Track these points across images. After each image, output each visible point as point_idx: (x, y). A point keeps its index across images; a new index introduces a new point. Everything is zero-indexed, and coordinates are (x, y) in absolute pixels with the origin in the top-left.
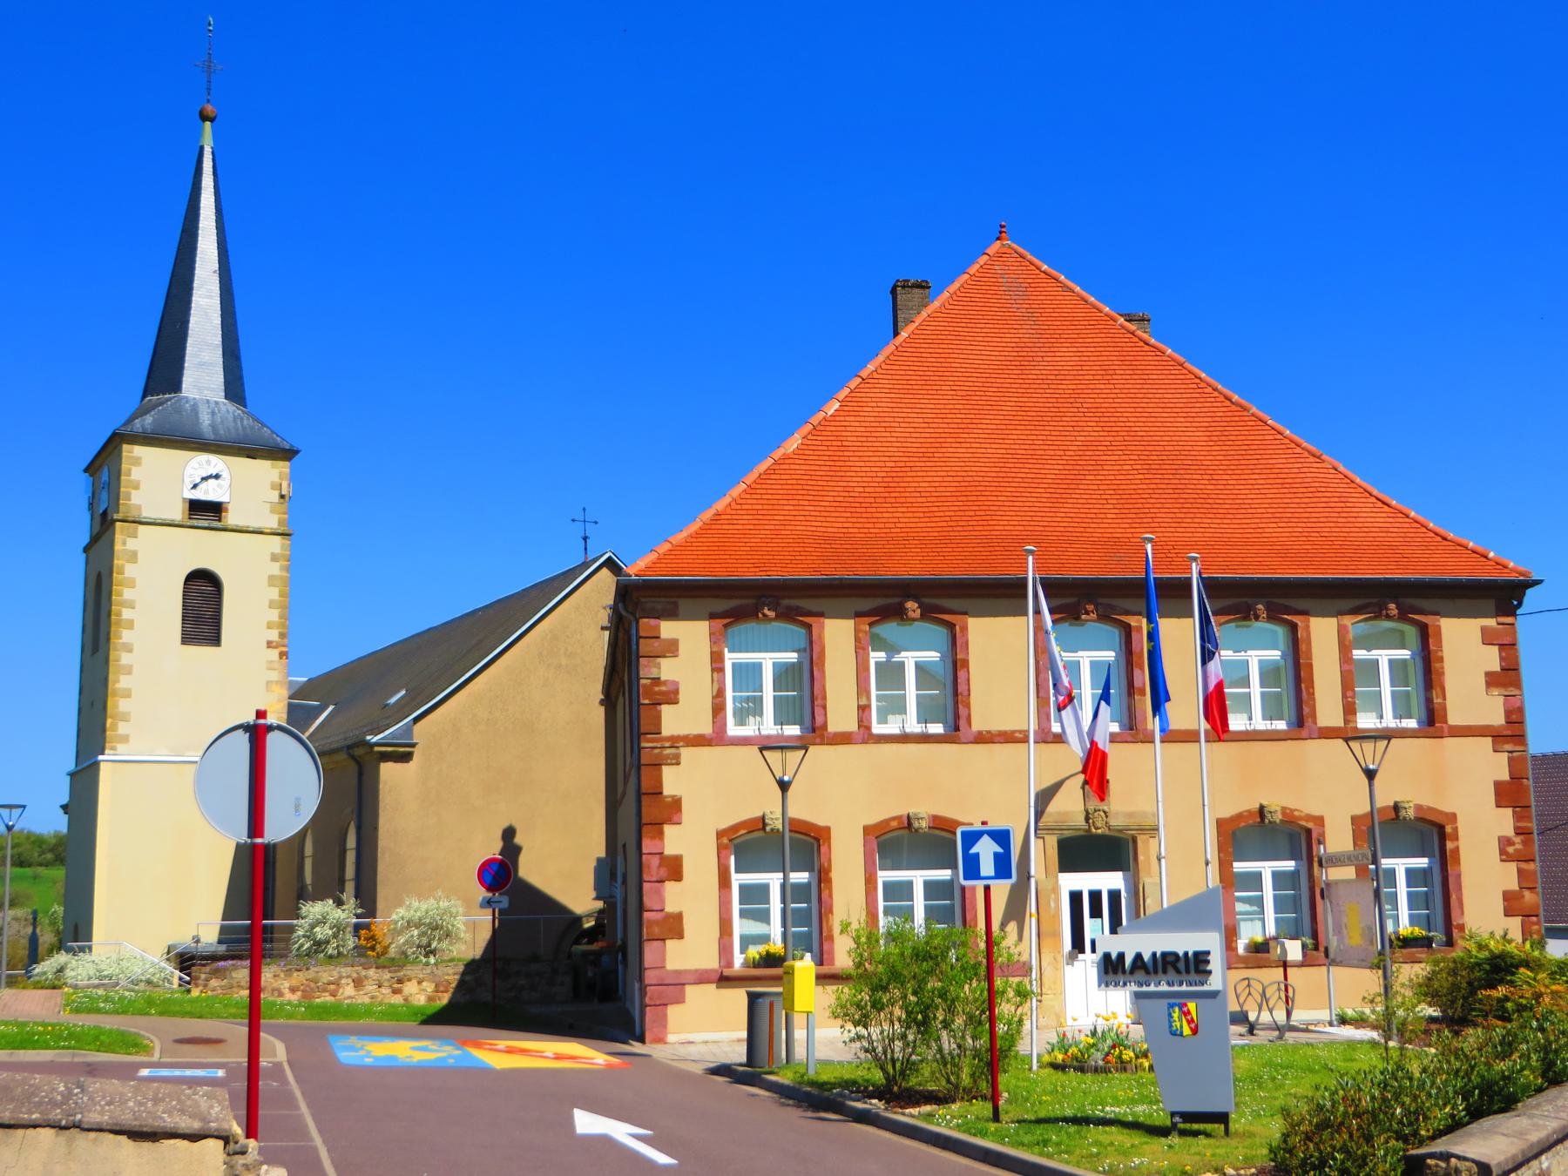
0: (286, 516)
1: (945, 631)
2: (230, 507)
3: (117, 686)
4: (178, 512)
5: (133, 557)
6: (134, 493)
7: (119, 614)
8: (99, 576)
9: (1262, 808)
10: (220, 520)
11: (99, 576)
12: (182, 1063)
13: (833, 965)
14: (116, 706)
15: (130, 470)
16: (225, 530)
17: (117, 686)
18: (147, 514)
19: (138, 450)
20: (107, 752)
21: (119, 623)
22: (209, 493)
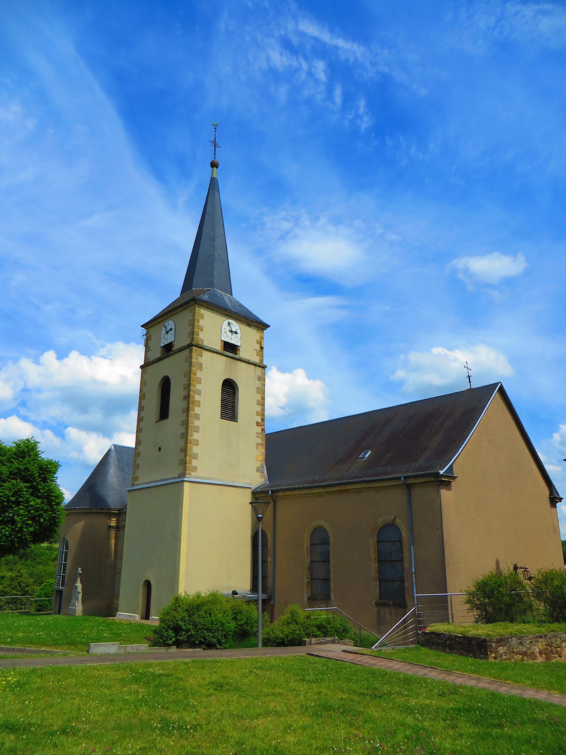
0: (6, 555)
1: (43, 456)
2: (241, 349)
3: (192, 438)
4: (218, 347)
5: (200, 367)
6: (200, 333)
7: (194, 397)
8: (164, 413)
9: (455, 478)
10: (236, 354)
11: (164, 413)
12: (160, 482)
13: (191, 464)
14: (191, 450)
15: (199, 320)
16: (240, 360)
17: (192, 438)
18: (206, 344)
19: (203, 311)
20: (187, 476)
21: (193, 402)
22: (234, 340)
